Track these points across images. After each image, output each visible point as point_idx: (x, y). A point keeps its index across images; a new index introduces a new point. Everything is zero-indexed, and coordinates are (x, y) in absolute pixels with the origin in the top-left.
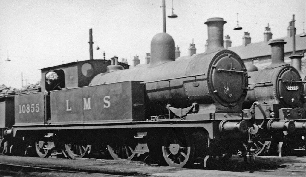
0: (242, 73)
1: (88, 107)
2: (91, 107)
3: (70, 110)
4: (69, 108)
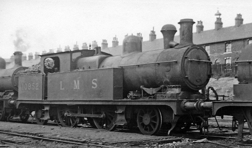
0: (208, 62)
1: (78, 87)
2: (80, 88)
3: (63, 89)
4: (62, 88)
